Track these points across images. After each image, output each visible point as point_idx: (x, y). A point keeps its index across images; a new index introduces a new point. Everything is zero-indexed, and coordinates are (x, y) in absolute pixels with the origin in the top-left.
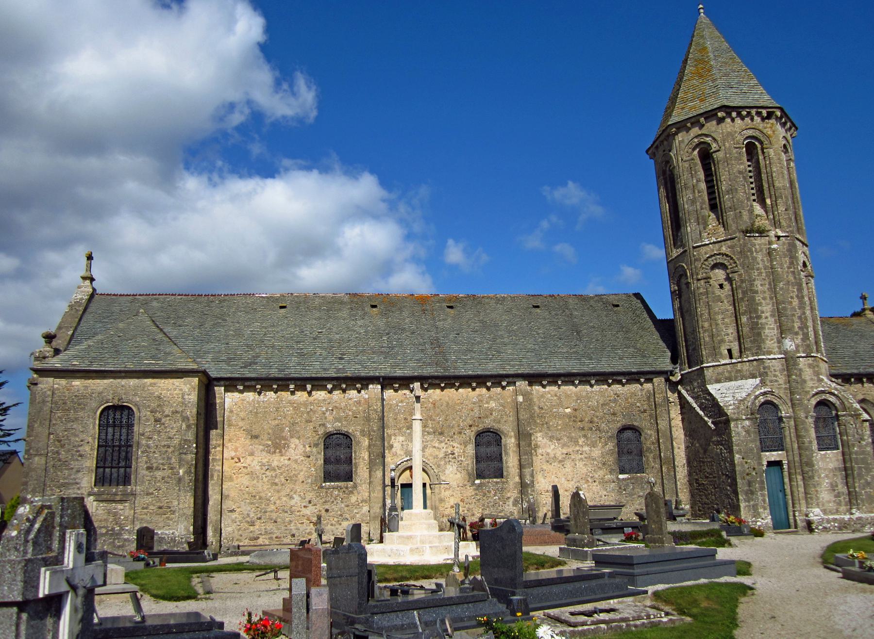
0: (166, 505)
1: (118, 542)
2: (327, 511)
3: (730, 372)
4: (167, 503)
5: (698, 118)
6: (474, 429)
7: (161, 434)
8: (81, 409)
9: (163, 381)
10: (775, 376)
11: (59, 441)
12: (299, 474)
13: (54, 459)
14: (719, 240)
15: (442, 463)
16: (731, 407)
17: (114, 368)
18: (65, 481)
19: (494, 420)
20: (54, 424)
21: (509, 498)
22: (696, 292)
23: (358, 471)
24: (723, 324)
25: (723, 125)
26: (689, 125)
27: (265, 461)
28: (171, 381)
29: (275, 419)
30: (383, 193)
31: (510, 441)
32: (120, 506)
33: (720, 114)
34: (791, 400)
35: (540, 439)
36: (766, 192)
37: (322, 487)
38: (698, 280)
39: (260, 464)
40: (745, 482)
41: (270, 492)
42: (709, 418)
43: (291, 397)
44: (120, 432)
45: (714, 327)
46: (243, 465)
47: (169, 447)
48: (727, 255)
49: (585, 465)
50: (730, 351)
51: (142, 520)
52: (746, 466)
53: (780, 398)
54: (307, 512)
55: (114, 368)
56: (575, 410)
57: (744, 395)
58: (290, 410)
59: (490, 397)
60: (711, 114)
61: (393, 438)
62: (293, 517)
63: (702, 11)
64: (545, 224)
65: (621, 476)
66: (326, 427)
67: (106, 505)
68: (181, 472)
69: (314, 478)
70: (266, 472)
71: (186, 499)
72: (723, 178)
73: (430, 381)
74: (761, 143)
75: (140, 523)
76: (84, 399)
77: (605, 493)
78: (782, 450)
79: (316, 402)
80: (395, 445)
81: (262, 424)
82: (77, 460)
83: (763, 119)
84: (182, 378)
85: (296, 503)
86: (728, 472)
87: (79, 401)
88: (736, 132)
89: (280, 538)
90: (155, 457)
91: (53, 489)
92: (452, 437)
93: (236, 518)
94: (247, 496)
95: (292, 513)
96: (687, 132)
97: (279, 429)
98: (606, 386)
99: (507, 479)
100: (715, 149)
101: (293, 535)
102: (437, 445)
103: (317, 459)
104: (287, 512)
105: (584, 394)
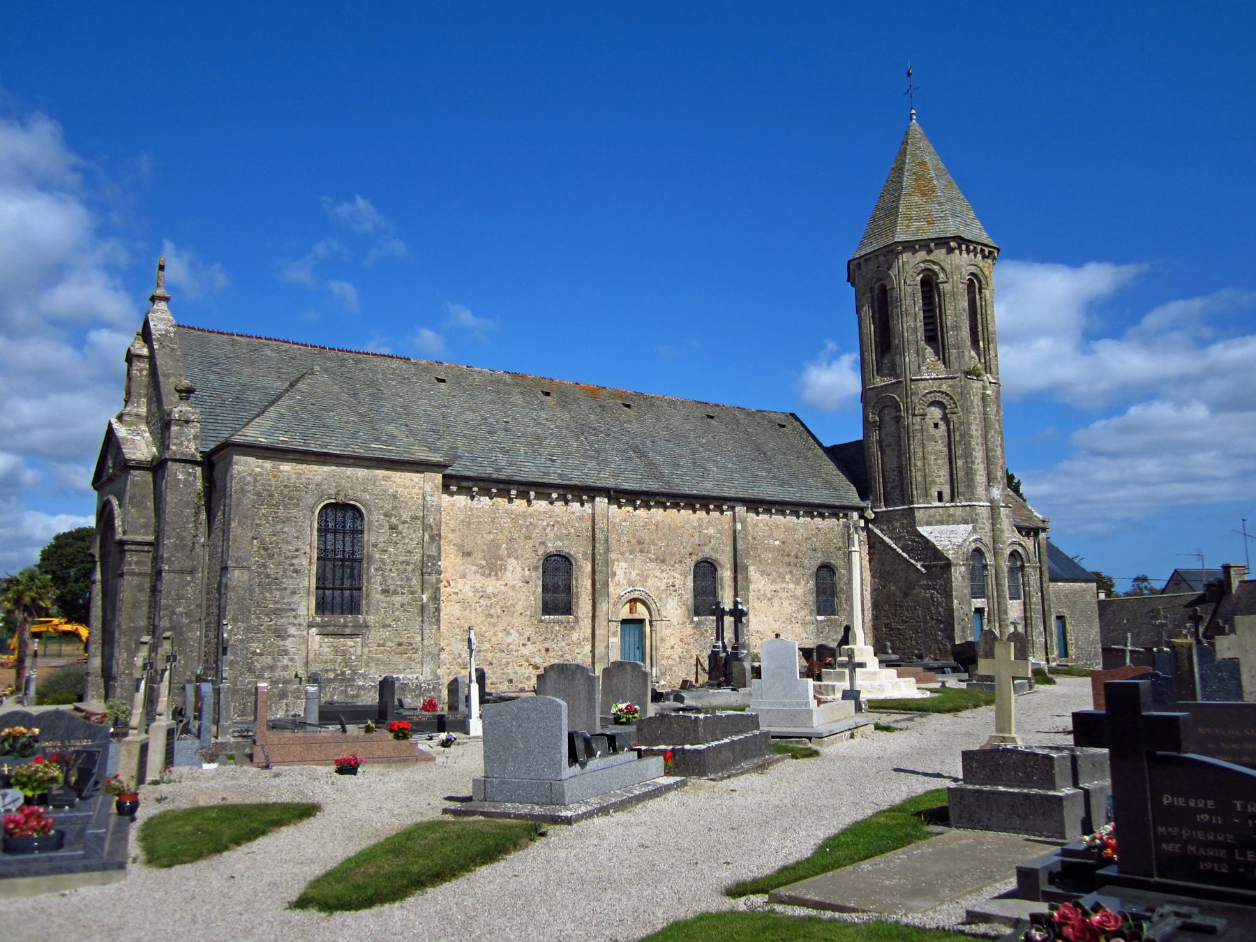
0: (406, 641)
1: (351, 691)
2: (547, 650)
4: (408, 637)
5: (928, 242)
6: (694, 557)
7: (398, 546)
8: (294, 504)
10: (983, 523)
11: (266, 549)
12: (516, 603)
13: (259, 574)
16: (950, 552)
17: (340, 450)
18: (276, 606)
20: (257, 525)
22: (911, 428)
23: (580, 603)
24: (935, 465)
25: (952, 255)
26: (917, 247)
27: (478, 586)
28: (409, 475)
30: (73, 159)
31: (726, 574)
32: (350, 643)
33: (953, 244)
34: (994, 549)
35: (752, 573)
36: (980, 337)
37: (542, 621)
38: (914, 415)
39: (473, 590)
40: (960, 627)
41: (484, 626)
42: (917, 561)
43: (508, 506)
44: (343, 541)
45: (926, 467)
46: (453, 590)
47: (408, 564)
48: (947, 395)
49: (790, 604)
51: (378, 660)
52: (962, 612)
53: (986, 545)
54: (525, 651)
55: (340, 450)
56: (784, 543)
57: (961, 540)
58: (506, 522)
59: (709, 522)
60: (943, 241)
61: (616, 563)
62: (510, 658)
63: (914, 117)
64: (321, 249)
65: (820, 618)
66: (546, 547)
67: (332, 640)
68: (425, 597)
70: (480, 601)
71: (431, 633)
72: (948, 312)
73: (657, 498)
74: (980, 282)
75: (376, 665)
76: (297, 491)
78: (984, 598)
79: (536, 513)
81: (475, 537)
82: (292, 577)
83: (984, 257)
84: (422, 472)
85: (514, 640)
86: (941, 616)
87: (291, 495)
88: (962, 266)
89: (496, 684)
91: (261, 618)
92: (673, 566)
93: (445, 659)
94: (457, 630)
95: (509, 652)
96: (913, 254)
97: (495, 545)
98: (809, 519)
100: (943, 280)
101: (511, 681)
102: (658, 574)
103: (536, 586)
104: (503, 651)
105: (791, 525)
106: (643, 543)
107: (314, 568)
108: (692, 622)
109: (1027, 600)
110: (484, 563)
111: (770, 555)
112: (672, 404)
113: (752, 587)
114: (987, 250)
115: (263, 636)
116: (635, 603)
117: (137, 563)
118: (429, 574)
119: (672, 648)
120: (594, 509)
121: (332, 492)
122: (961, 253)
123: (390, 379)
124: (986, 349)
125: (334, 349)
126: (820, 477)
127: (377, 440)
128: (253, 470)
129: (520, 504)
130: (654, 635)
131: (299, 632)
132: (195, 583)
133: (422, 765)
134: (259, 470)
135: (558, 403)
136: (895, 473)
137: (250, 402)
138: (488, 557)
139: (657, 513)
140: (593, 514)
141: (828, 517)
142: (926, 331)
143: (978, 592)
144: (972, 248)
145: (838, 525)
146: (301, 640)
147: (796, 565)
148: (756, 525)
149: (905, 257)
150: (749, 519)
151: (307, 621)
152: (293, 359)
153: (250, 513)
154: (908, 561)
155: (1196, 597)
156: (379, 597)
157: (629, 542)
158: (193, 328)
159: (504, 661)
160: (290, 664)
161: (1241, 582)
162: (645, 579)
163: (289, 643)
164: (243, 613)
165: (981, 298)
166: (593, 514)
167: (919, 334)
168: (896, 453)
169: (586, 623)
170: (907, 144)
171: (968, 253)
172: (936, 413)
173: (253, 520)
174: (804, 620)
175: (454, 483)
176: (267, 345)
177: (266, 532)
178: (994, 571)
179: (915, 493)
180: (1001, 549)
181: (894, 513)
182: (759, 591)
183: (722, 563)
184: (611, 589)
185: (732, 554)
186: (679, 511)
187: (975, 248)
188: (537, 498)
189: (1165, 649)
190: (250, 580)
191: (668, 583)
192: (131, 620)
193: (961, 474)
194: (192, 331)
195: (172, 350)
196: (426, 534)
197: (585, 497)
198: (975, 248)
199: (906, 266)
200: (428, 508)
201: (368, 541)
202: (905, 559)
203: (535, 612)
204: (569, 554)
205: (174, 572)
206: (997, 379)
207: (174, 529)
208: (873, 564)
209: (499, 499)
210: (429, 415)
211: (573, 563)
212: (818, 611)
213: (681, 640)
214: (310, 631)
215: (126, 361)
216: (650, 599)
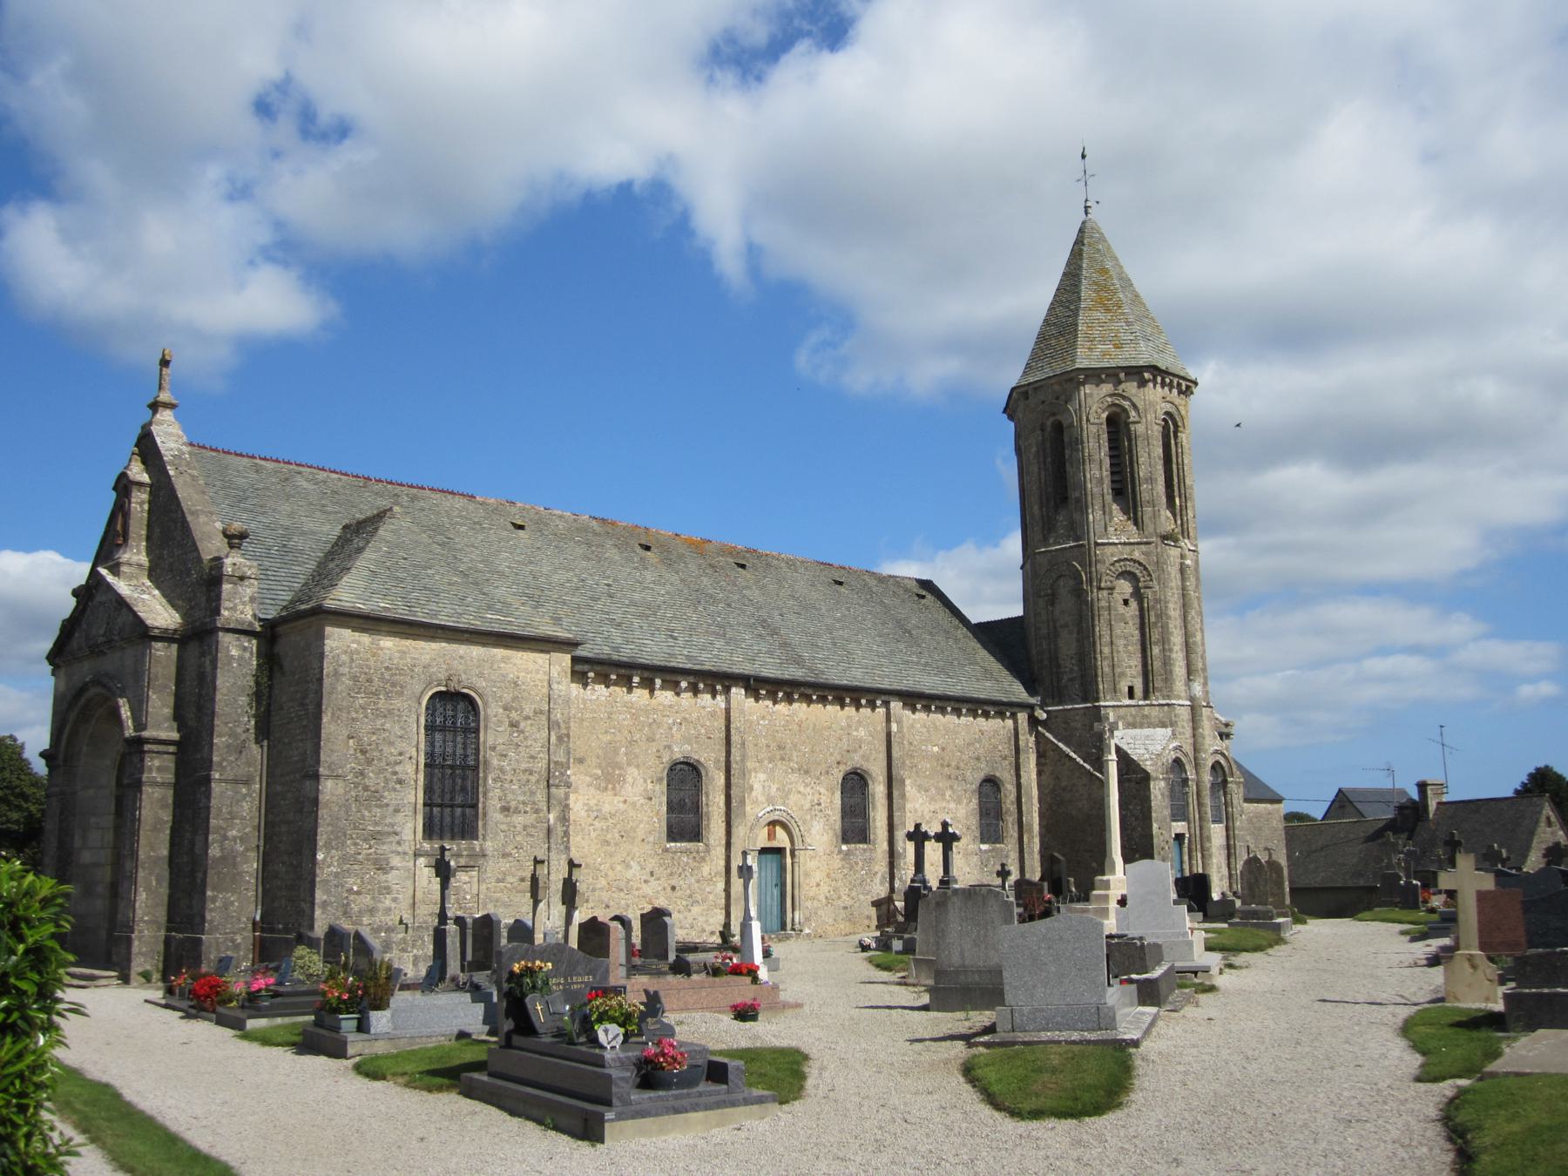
2: (673, 888)
3: (1134, 717)
5: (1118, 370)
7: (521, 749)
8: (397, 693)
9: (520, 654)
10: (1183, 727)
12: (637, 827)
13: (356, 785)
14: (1132, 541)
15: (808, 817)
16: (1148, 763)
17: (454, 622)
19: (863, 756)
20: (353, 719)
21: (876, 873)
22: (1096, 604)
23: (711, 826)
25: (1146, 389)
26: (1103, 376)
27: (593, 802)
29: (606, 733)
31: (878, 789)
33: (1146, 375)
34: (1195, 759)
36: (1176, 493)
38: (1100, 588)
45: (1115, 654)
48: (1140, 564)
50: (1131, 689)
51: (497, 901)
52: (1162, 838)
53: (1186, 755)
55: (454, 622)
57: (1159, 748)
58: (625, 719)
59: (859, 722)
61: (753, 774)
66: (672, 752)
69: (657, 835)
72: (1141, 460)
73: (802, 689)
76: (400, 674)
77: (968, 869)
78: (1184, 821)
79: (661, 707)
80: (755, 786)
82: (395, 790)
83: (1180, 392)
84: (548, 652)
85: (635, 875)
90: (513, 790)
92: (818, 779)
98: (971, 719)
99: (874, 845)
102: (802, 789)
103: (660, 804)
104: (622, 890)
105: (952, 726)
106: (784, 748)
107: (421, 777)
108: (840, 851)
109: (1231, 824)
110: (599, 772)
111: (928, 766)
112: (791, 564)
113: (908, 806)
114: (1184, 383)
115: (361, 869)
116: (774, 827)
117: (159, 769)
118: (557, 786)
119: (818, 885)
120: (728, 702)
121: (442, 676)
122: (1155, 387)
123: (458, 523)
124: (1184, 508)
125: (380, 481)
126: (977, 664)
127: (490, 608)
128: (349, 646)
129: (640, 695)
130: (796, 868)
131: (405, 864)
132: (251, 796)
133: (789, 1013)
134: (355, 646)
135: (662, 561)
136: (1073, 661)
137: (301, 552)
138: (604, 764)
139: (800, 708)
140: (728, 711)
141: (993, 717)
142: (1113, 482)
143: (1179, 813)
144: (1167, 380)
145: (1004, 727)
146: (406, 874)
147: (957, 779)
148: (912, 726)
149: (1088, 389)
150: (904, 719)
151: (413, 848)
152: (336, 493)
153: (344, 704)
154: (1092, 774)
155: (1384, 822)
156: (498, 816)
157: (768, 746)
158: (204, 447)
159: (623, 902)
160: (393, 905)
161: (1439, 803)
162: (786, 795)
163: (392, 877)
164: (337, 838)
165: (1176, 444)
166: (728, 711)
167: (1105, 486)
168: (1075, 635)
169: (720, 851)
170: (1083, 245)
171: (1163, 387)
172: (1125, 587)
173: (349, 712)
174: (966, 849)
175: (590, 669)
176: (300, 473)
177: (364, 728)
178: (1195, 787)
179: (1101, 687)
180: (1203, 759)
181: (1072, 713)
182: (916, 811)
183: (874, 775)
184: (748, 808)
185: (885, 764)
186: (825, 706)
187: (1171, 381)
188: (663, 688)
189: (1414, 882)
190: (346, 793)
191: (812, 801)
192: (152, 849)
193: (1157, 664)
194: (204, 451)
195: (193, 477)
196: (552, 733)
197: (719, 687)
198: (1171, 381)
199: (1089, 400)
200: (555, 700)
201: (485, 742)
202: (1089, 771)
203: (659, 838)
204: (698, 761)
205: (226, 781)
206: (1196, 546)
207: (226, 723)
208: (1043, 777)
209: (617, 689)
210: (517, 574)
211: (703, 773)
212: (843, 839)
213: (828, 876)
214: (417, 862)
215: (115, 488)
216: (793, 821)
